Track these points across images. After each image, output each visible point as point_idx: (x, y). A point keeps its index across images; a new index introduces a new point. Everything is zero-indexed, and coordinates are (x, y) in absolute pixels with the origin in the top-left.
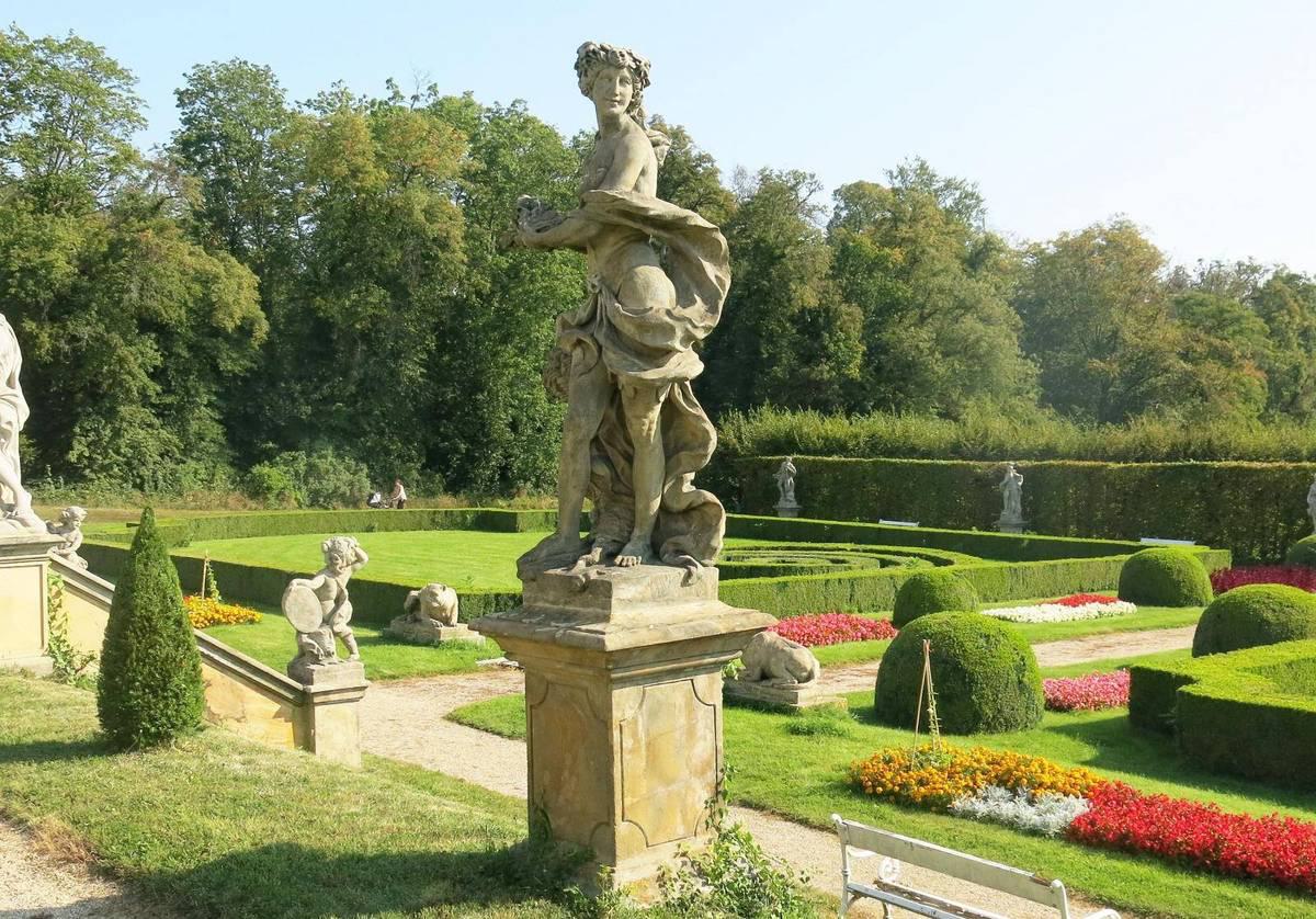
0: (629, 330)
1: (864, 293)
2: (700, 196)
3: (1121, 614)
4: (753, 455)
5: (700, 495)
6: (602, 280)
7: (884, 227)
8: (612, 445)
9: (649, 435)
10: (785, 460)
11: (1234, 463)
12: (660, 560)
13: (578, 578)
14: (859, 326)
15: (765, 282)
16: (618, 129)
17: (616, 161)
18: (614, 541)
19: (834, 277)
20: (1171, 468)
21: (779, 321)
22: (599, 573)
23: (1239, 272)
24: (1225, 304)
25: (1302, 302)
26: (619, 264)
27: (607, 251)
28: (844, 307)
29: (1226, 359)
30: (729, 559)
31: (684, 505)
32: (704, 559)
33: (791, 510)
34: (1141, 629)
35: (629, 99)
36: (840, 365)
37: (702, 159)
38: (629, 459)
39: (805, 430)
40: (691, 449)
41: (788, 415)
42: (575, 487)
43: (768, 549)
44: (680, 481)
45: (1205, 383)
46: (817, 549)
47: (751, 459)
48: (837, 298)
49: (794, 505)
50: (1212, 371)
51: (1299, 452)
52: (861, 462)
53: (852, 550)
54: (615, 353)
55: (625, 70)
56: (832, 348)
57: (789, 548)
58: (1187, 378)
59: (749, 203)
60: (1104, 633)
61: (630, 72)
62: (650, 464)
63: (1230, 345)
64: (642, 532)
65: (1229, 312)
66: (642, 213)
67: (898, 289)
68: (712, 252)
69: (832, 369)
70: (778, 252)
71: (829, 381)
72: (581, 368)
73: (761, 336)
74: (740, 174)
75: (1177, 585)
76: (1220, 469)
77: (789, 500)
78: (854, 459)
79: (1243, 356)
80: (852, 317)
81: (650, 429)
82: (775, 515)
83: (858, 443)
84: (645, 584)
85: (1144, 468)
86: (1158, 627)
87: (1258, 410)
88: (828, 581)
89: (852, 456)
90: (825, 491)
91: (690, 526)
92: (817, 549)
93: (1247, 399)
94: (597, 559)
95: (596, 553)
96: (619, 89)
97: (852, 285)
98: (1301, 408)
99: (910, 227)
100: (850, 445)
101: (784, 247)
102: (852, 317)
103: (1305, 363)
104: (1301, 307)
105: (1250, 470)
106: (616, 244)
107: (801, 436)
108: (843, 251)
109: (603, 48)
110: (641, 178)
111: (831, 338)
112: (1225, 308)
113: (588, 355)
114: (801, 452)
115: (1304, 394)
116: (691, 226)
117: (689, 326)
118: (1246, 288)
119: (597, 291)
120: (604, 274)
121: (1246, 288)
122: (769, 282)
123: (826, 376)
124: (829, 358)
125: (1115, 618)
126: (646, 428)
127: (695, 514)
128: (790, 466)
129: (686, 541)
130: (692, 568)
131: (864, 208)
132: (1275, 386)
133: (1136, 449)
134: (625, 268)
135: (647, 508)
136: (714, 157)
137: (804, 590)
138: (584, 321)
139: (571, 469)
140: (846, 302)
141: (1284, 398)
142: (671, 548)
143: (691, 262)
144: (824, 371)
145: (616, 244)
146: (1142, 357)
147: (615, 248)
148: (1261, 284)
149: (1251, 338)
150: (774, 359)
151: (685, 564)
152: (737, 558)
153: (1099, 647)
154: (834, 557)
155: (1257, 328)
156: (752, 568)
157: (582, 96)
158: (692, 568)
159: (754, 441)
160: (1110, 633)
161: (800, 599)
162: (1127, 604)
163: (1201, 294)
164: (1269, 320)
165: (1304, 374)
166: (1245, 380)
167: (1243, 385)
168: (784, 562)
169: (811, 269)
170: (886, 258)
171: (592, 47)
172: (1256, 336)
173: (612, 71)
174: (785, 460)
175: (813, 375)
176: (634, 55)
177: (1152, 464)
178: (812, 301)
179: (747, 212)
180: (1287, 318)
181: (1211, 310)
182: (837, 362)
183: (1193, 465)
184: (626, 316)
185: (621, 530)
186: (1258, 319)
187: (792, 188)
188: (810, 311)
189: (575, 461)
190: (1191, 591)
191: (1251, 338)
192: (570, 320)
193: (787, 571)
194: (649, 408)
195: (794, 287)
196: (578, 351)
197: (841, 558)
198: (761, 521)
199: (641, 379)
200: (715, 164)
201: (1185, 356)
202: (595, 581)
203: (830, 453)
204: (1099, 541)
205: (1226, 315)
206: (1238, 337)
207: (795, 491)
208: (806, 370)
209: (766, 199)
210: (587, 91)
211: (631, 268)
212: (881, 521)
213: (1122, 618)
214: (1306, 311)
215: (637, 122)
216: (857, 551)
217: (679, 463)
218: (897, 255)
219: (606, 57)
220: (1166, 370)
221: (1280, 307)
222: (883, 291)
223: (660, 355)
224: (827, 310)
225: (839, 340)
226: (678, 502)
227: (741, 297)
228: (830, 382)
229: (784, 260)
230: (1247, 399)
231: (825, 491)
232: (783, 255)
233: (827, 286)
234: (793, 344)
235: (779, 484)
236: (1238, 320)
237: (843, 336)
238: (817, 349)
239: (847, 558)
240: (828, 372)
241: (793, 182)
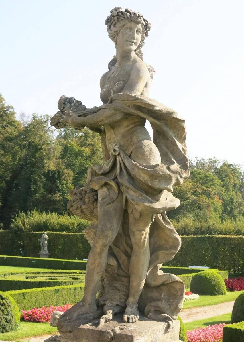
0: (143, 178)
1: (74, 165)
2: (7, 123)
3: (194, 299)
4: (29, 231)
5: (171, 277)
6: (121, 147)
7: (82, 139)
8: (122, 248)
9: (144, 241)
10: (44, 233)
11: (223, 236)
12: (147, 317)
13: (108, 333)
14: (71, 178)
15: (34, 159)
16: (129, 60)
17: (131, 77)
18: (117, 305)
19: (62, 158)
20: (200, 237)
21: (39, 175)
22: (121, 329)
23: (210, 162)
24: (207, 174)
25: (233, 174)
26: (131, 138)
27: (122, 130)
28: (66, 171)
29: (208, 194)
30: (27, 278)
31: (159, 282)
32: (173, 315)
33: (46, 254)
34: (203, 306)
35: (139, 43)
36: (63, 194)
37: (8, 108)
38: (129, 256)
39: (52, 221)
40: (166, 249)
41: (44, 215)
42: (98, 273)
43: (43, 273)
44: (156, 268)
45: (201, 204)
46: (64, 273)
47: (28, 233)
48: (63, 167)
49: (47, 252)
50: (204, 198)
51: (240, 231)
52: (76, 235)
53: (80, 273)
54: (135, 192)
55: (140, 25)
56: (60, 187)
57: (52, 273)
58: (194, 202)
59: (27, 127)
60: (190, 308)
61: (142, 27)
62: (143, 258)
63: (210, 189)
64: (133, 300)
65: (209, 177)
66: (151, 108)
67: (87, 164)
68: (178, 134)
69: (60, 195)
70: (39, 147)
71: (59, 200)
72: (107, 200)
73: (31, 181)
74: (23, 115)
75: (213, 286)
76: (219, 238)
77: (45, 250)
78: (73, 233)
79: (214, 194)
80: (69, 174)
81: (145, 238)
82: (39, 257)
83: (74, 226)
84: (148, 335)
85: (190, 237)
86: (209, 304)
87: (220, 214)
88: (76, 288)
89: (71, 232)
90: (60, 247)
91: (161, 295)
92: (64, 273)
93: (216, 210)
94: (111, 318)
95: (110, 315)
96: (136, 36)
97: (69, 162)
98: (234, 214)
99: (92, 140)
100: (71, 227)
101: (42, 145)
102: (69, 174)
103: (235, 197)
104: (233, 176)
105: (229, 238)
106: (127, 126)
107: (50, 223)
108: (65, 148)
109: (127, 11)
110: (145, 89)
111: (60, 183)
112: (208, 175)
113: (111, 192)
114: (50, 230)
115: (235, 209)
116: (174, 118)
117: (179, 177)
118: (213, 168)
119: (117, 153)
120: (122, 144)
121: (213, 168)
122: (35, 159)
123: (58, 198)
124: (59, 191)
125: (192, 301)
126: (143, 237)
127: (164, 288)
128: (46, 236)
129: (163, 305)
130: (170, 322)
131: (71, 131)
132: (225, 206)
133: (182, 230)
134: (135, 140)
135: (139, 284)
136: (14, 107)
137: (66, 292)
138: (106, 171)
139: (97, 262)
140: (66, 168)
141: (228, 211)
142: (152, 309)
143: (168, 139)
144: (57, 196)
145: (127, 126)
146: (179, 194)
147: (128, 128)
148: (219, 167)
149: (217, 187)
150: (35, 191)
151: (165, 320)
152: (31, 278)
153: (191, 314)
154: (73, 277)
155: (219, 184)
156: (40, 282)
157: (108, 37)
158: (170, 322)
159: (30, 225)
160: (192, 308)
161: (64, 297)
162: (195, 295)
163: (199, 170)
164: (223, 181)
165: (235, 201)
166: (215, 203)
167: (214, 205)
168: (51, 279)
169: (52, 155)
170: (83, 151)
171: (121, 10)
172: (218, 186)
173: (133, 24)
174: (44, 233)
175: (53, 198)
176: (144, 17)
177: (193, 236)
178: (53, 167)
179: (27, 130)
180: (229, 180)
181: (202, 176)
182: (63, 193)
183: (208, 237)
184: (143, 170)
185: (121, 298)
186: (219, 180)
187: (45, 122)
188: (52, 172)
189: (100, 258)
190: (219, 289)
191: (217, 187)
192: (97, 171)
193: (56, 284)
194: (146, 226)
195: (46, 162)
196: (105, 189)
197: (76, 277)
198: (35, 260)
199: (153, 208)
200: (14, 110)
201: (194, 193)
202: (120, 335)
203: (62, 231)
204: (172, 267)
205: (208, 178)
206: (212, 187)
207: (48, 247)
208: (50, 196)
209: (35, 126)
210: (113, 37)
211: (140, 141)
212: (84, 259)
213: (195, 301)
214: (235, 178)
215: (139, 57)
216: (81, 273)
217: (157, 258)
218: (87, 151)
219: (130, 16)
220: (187, 199)
221: (226, 176)
222: (81, 164)
223: (155, 193)
224: (59, 172)
225: (63, 184)
226: (155, 280)
227: (22, 165)
228: (60, 201)
229: (42, 150)
230: (216, 210)
231: (60, 247)
232: (41, 149)
233: (59, 162)
234: (44, 185)
235: (41, 244)
236: (212, 180)
237: (65, 182)
238: (54, 188)
239: (78, 277)
240: (59, 197)
241: (46, 119)
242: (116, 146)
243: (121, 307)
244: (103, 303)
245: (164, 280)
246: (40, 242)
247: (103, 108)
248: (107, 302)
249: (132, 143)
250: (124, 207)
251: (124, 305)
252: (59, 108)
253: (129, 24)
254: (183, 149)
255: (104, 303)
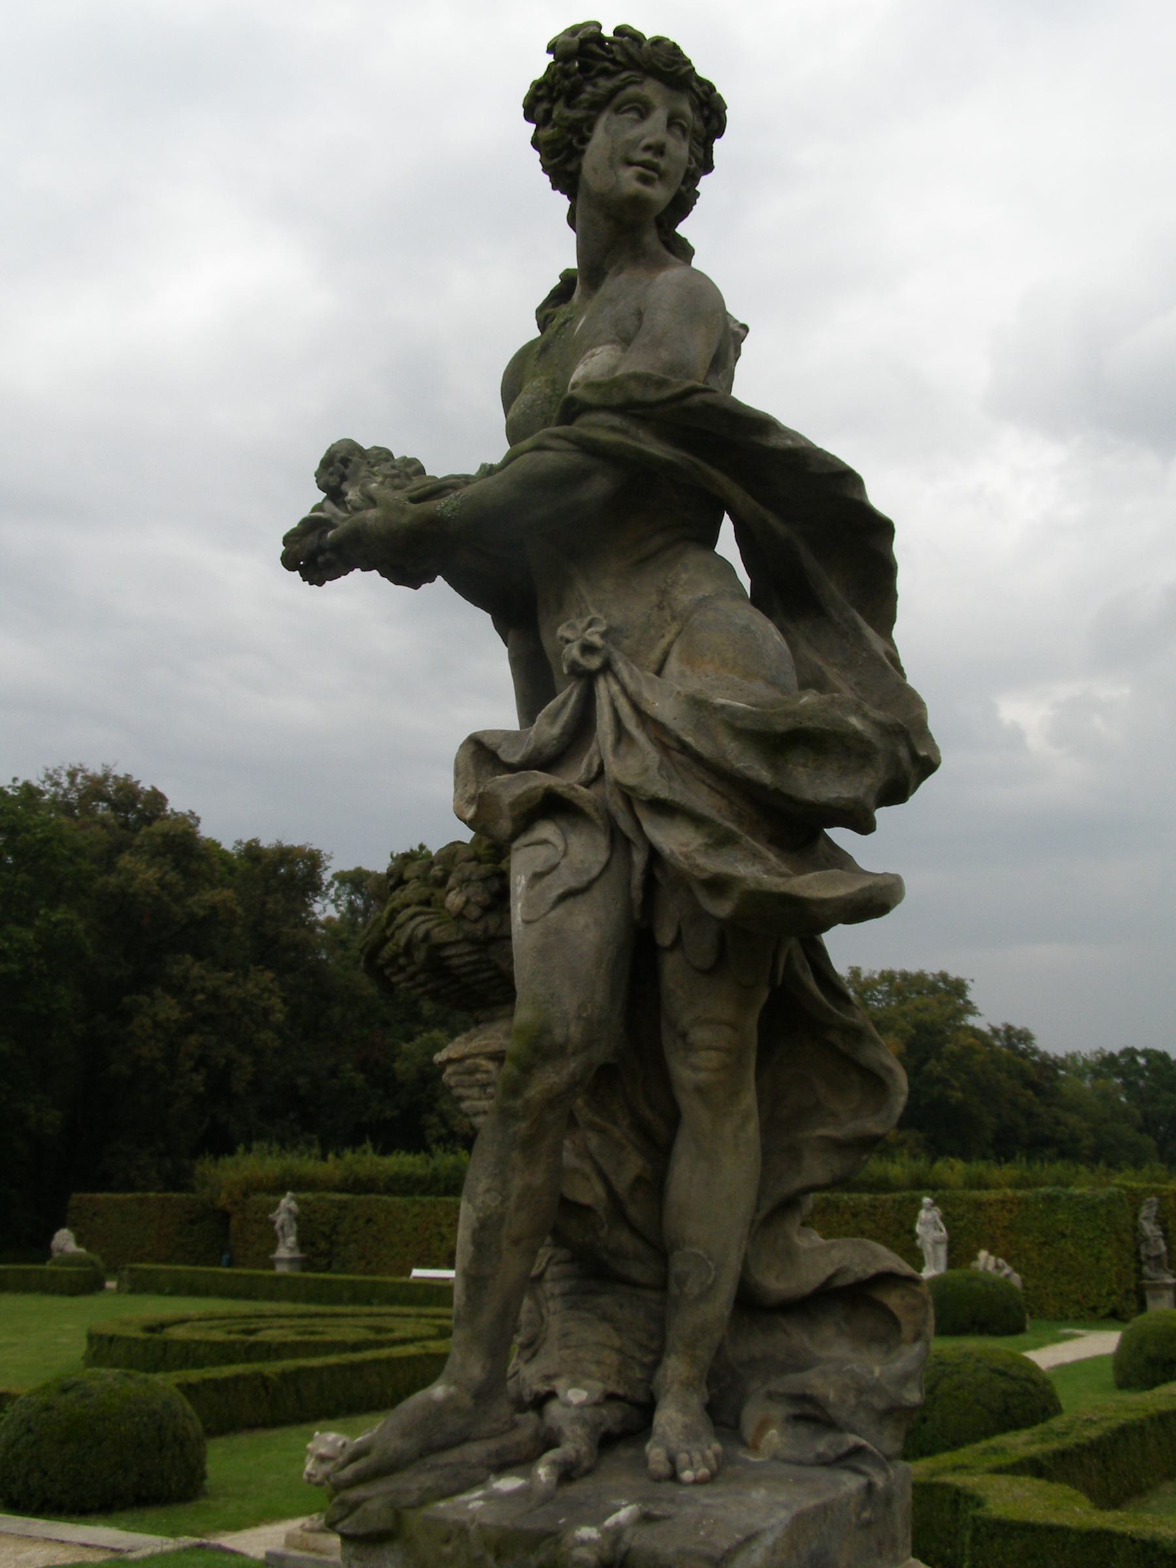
30: (230, 1332)
138: (548, 751)
242: (590, 630)
243: (626, 1406)
244: (543, 1388)
245: (830, 1271)
246: (274, 1223)
247: (337, 1517)
248: (560, 1385)
249: (667, 614)
250: (637, 916)
251: (640, 1396)
252: (322, 488)
253: (632, 90)
254: (887, 653)
255: (547, 1388)
